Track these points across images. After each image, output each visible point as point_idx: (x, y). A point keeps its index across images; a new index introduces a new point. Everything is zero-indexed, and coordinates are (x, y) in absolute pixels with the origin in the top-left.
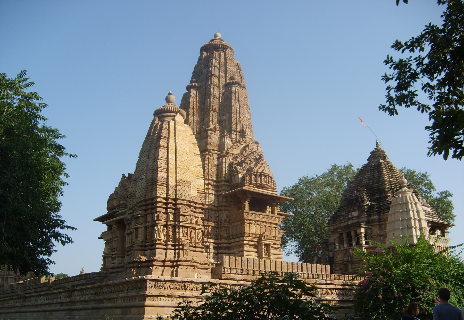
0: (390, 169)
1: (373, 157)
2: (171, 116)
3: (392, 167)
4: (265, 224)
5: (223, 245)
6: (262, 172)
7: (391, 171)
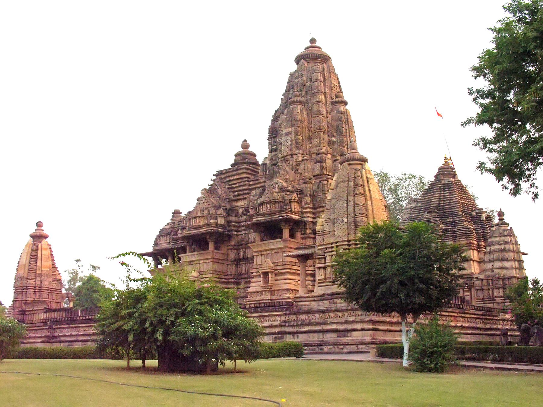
0: (461, 189)
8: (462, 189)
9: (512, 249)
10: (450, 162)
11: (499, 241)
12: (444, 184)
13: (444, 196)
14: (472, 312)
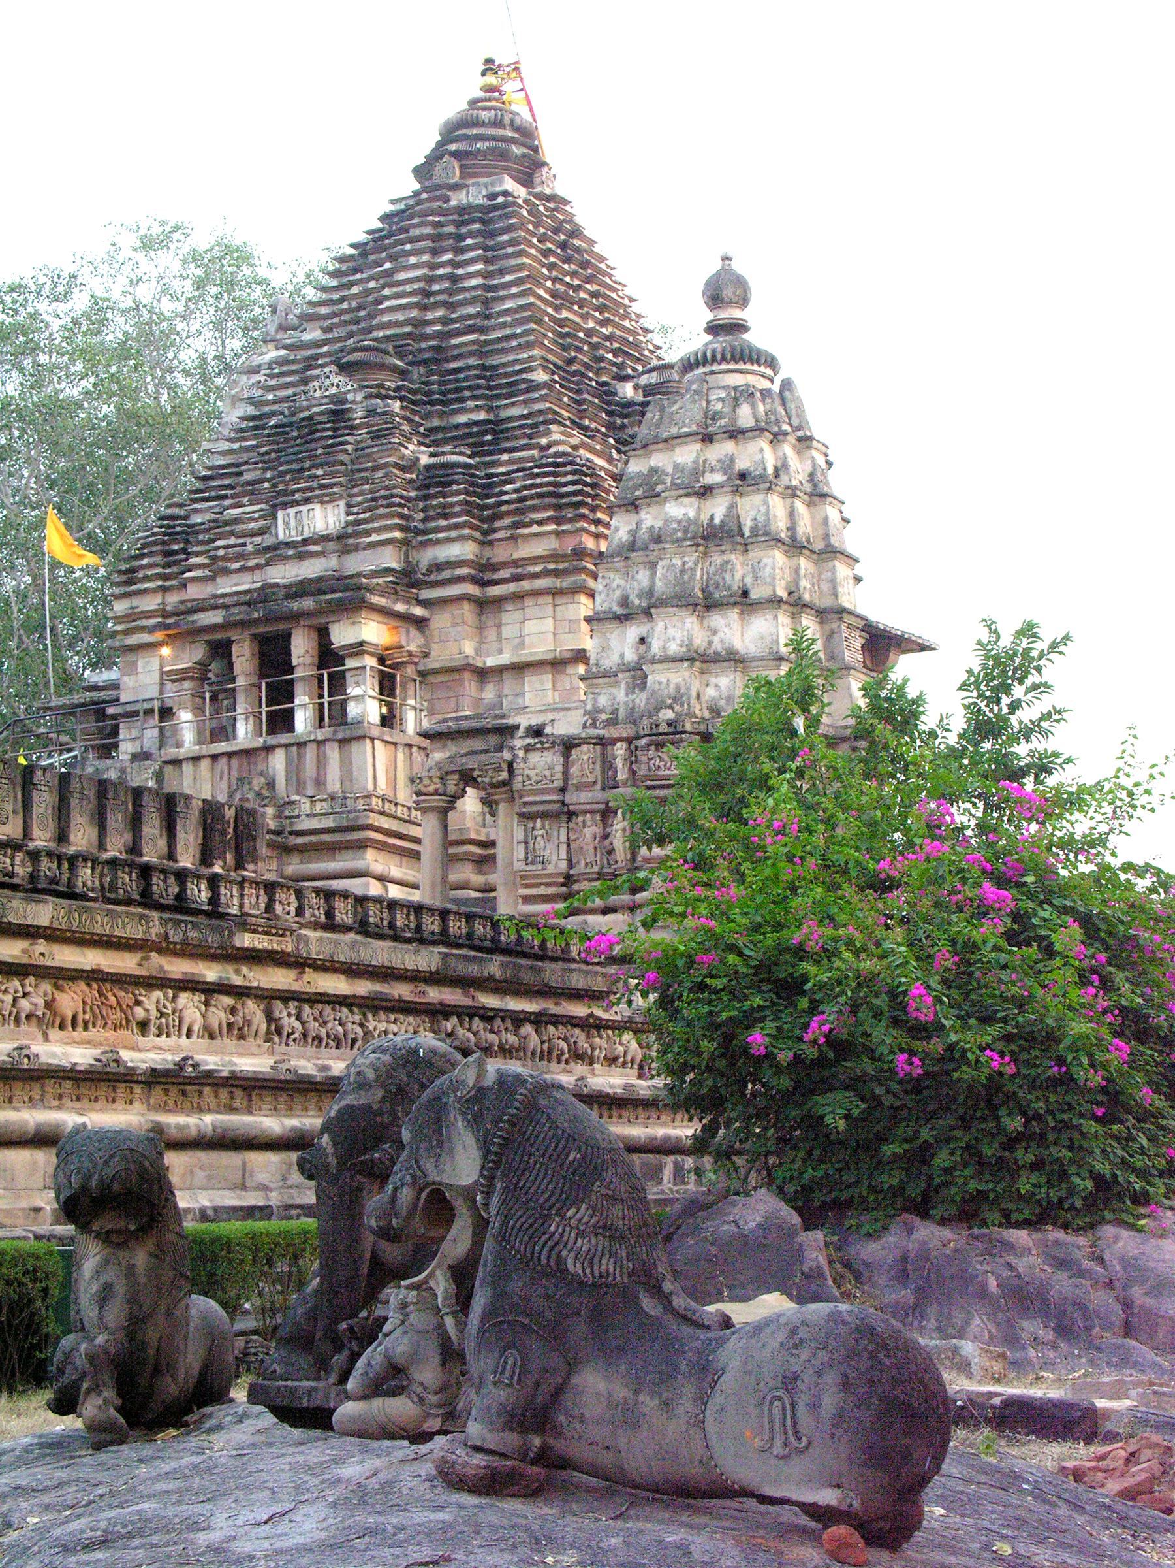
0: (563, 246)
1: (456, 155)
3: (576, 233)
7: (568, 260)
8: (568, 245)
9: (781, 524)
10: (509, 87)
11: (697, 471)
12: (462, 210)
13: (453, 278)
14: (316, 942)
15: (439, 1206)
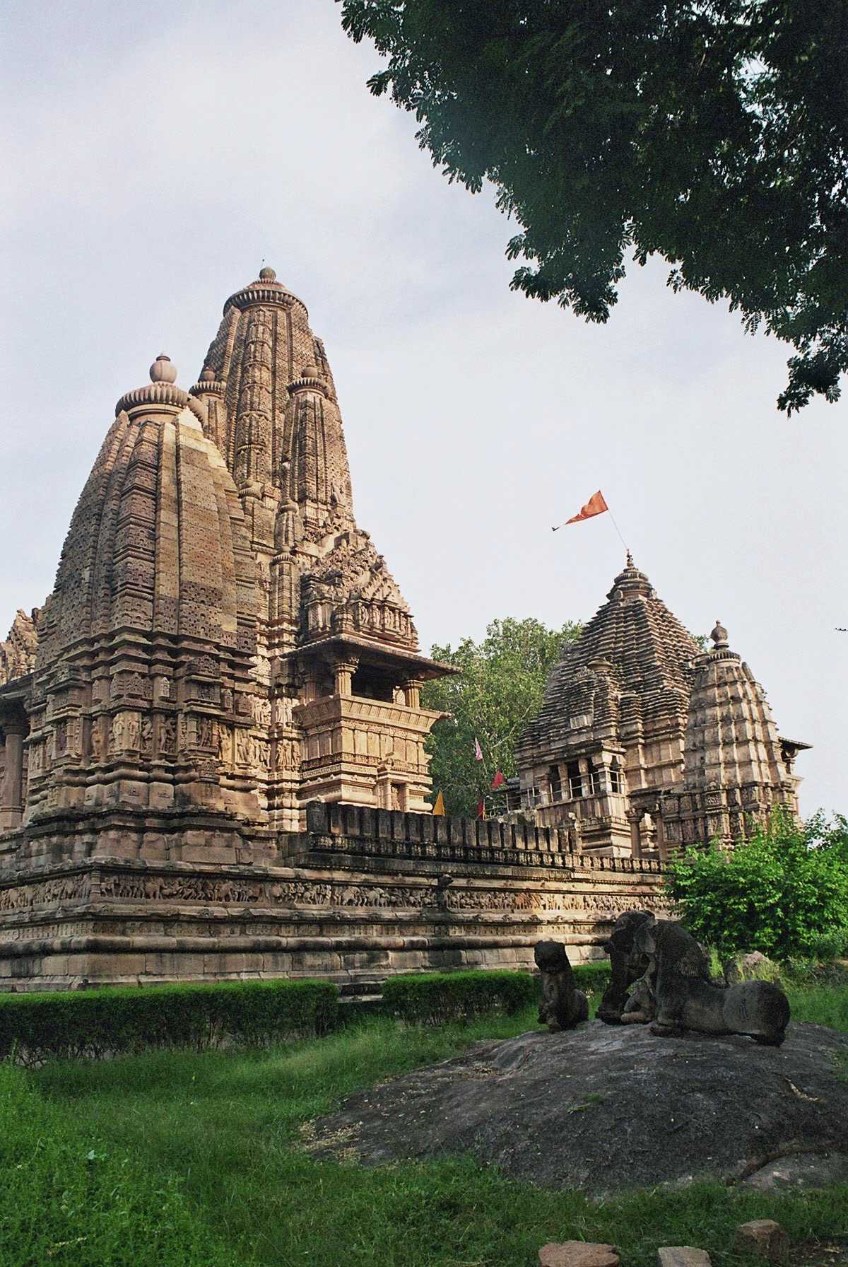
2: (165, 413)
3: (666, 612)
4: (391, 731)
5: (284, 785)
6: (385, 600)
15: (646, 959)
